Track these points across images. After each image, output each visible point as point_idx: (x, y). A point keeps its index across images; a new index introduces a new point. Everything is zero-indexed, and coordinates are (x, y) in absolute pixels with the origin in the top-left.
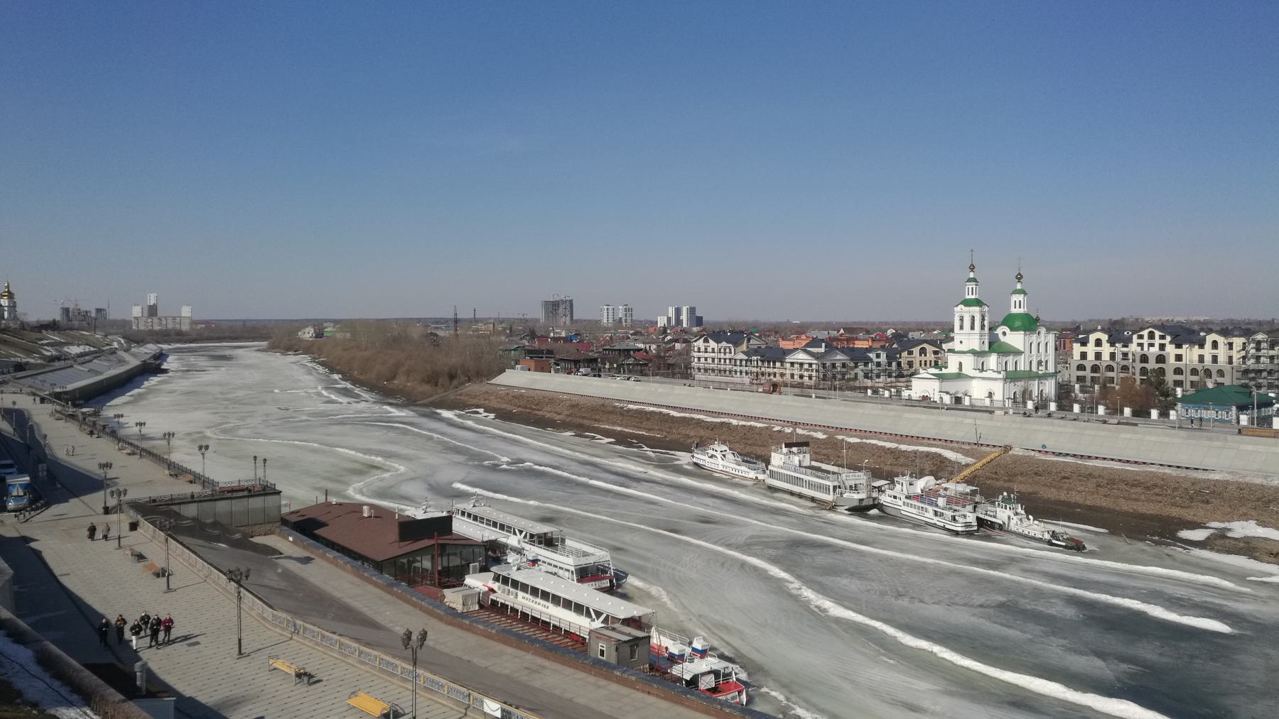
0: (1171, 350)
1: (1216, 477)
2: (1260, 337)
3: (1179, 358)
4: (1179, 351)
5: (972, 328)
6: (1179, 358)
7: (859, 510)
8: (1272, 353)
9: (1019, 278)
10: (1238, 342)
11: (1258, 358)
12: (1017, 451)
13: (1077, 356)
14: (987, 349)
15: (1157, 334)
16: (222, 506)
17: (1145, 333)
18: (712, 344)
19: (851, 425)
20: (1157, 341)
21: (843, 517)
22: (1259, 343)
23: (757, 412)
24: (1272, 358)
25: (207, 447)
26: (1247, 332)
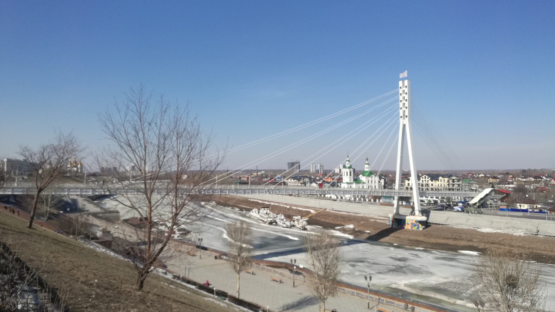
0: (430, 182)
1: (360, 215)
2: (454, 178)
3: (432, 185)
4: (432, 183)
5: (350, 175)
6: (432, 185)
7: (271, 223)
8: (458, 183)
9: (367, 160)
10: (446, 179)
11: (453, 185)
12: (327, 210)
13: (407, 185)
14: (352, 181)
15: (427, 177)
16: (107, 215)
17: (424, 177)
18: (292, 180)
19: (295, 204)
20: (427, 179)
21: (267, 225)
22: (453, 180)
23: (275, 200)
24: (459, 185)
25: (202, 240)
26: (449, 176)
